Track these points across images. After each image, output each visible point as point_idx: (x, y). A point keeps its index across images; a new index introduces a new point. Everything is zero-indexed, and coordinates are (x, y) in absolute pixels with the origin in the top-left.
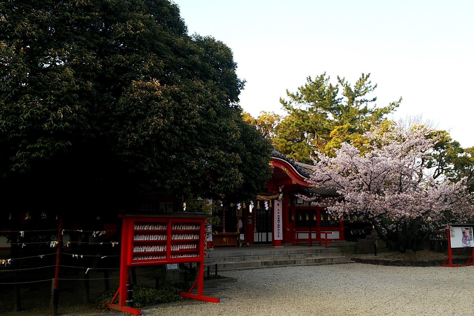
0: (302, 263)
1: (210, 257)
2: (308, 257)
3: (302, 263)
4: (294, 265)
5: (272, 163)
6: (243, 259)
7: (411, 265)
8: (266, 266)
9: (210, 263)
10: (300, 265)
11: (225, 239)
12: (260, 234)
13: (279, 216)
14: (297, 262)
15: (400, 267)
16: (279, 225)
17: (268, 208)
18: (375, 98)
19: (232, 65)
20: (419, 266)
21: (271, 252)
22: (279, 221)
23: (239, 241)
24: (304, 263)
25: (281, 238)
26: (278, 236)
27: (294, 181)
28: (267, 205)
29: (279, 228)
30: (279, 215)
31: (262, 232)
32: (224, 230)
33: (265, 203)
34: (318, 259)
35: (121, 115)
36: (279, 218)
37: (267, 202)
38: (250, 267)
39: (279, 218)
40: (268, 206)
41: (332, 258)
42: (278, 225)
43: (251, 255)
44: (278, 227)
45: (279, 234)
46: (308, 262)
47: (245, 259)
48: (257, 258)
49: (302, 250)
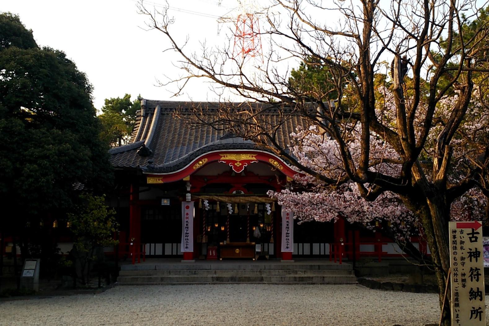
0: (274, 280)
1: (157, 269)
2: (290, 274)
3: (274, 280)
4: (261, 282)
5: (255, 157)
6: (194, 273)
7: (401, 290)
8: (218, 282)
9: (150, 275)
10: (271, 282)
11: (237, 251)
12: (301, 245)
13: (288, 222)
14: (264, 279)
15: (388, 292)
16: (289, 234)
17: (270, 211)
18: (138, 95)
19: (74, 66)
20: (411, 292)
21: (240, 266)
22: (288, 228)
23: (255, 253)
24: (277, 281)
25: (191, 250)
26: (287, 248)
27: (288, 176)
28: (270, 208)
29: (289, 238)
30: (288, 220)
31: (303, 242)
32: (248, 239)
33: (266, 206)
34: (299, 277)
35: (128, 107)
36: (288, 225)
37: (269, 205)
38: (196, 282)
39: (288, 225)
40: (271, 210)
41: (324, 277)
42: (187, 233)
43: (212, 268)
44: (286, 236)
45: (287, 245)
46: (283, 280)
47: (197, 273)
48: (214, 272)
49: (287, 265)
